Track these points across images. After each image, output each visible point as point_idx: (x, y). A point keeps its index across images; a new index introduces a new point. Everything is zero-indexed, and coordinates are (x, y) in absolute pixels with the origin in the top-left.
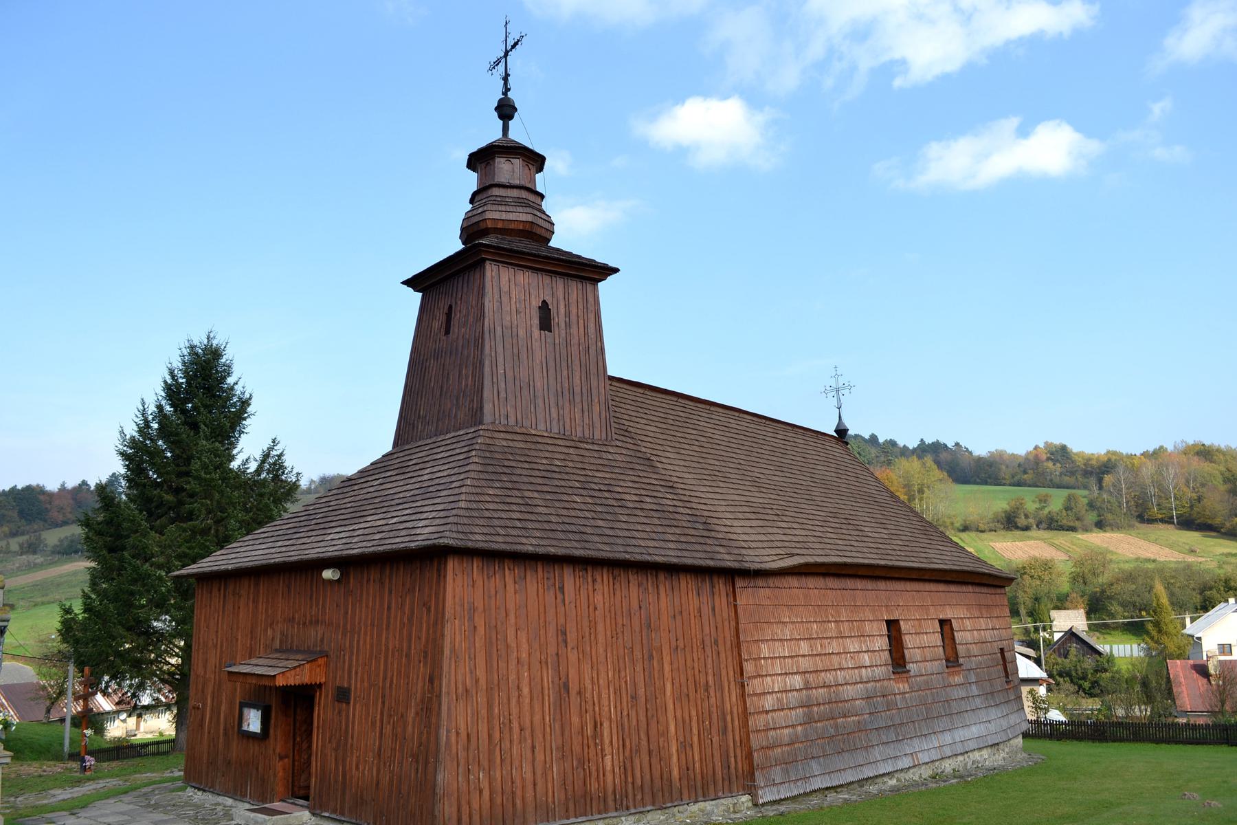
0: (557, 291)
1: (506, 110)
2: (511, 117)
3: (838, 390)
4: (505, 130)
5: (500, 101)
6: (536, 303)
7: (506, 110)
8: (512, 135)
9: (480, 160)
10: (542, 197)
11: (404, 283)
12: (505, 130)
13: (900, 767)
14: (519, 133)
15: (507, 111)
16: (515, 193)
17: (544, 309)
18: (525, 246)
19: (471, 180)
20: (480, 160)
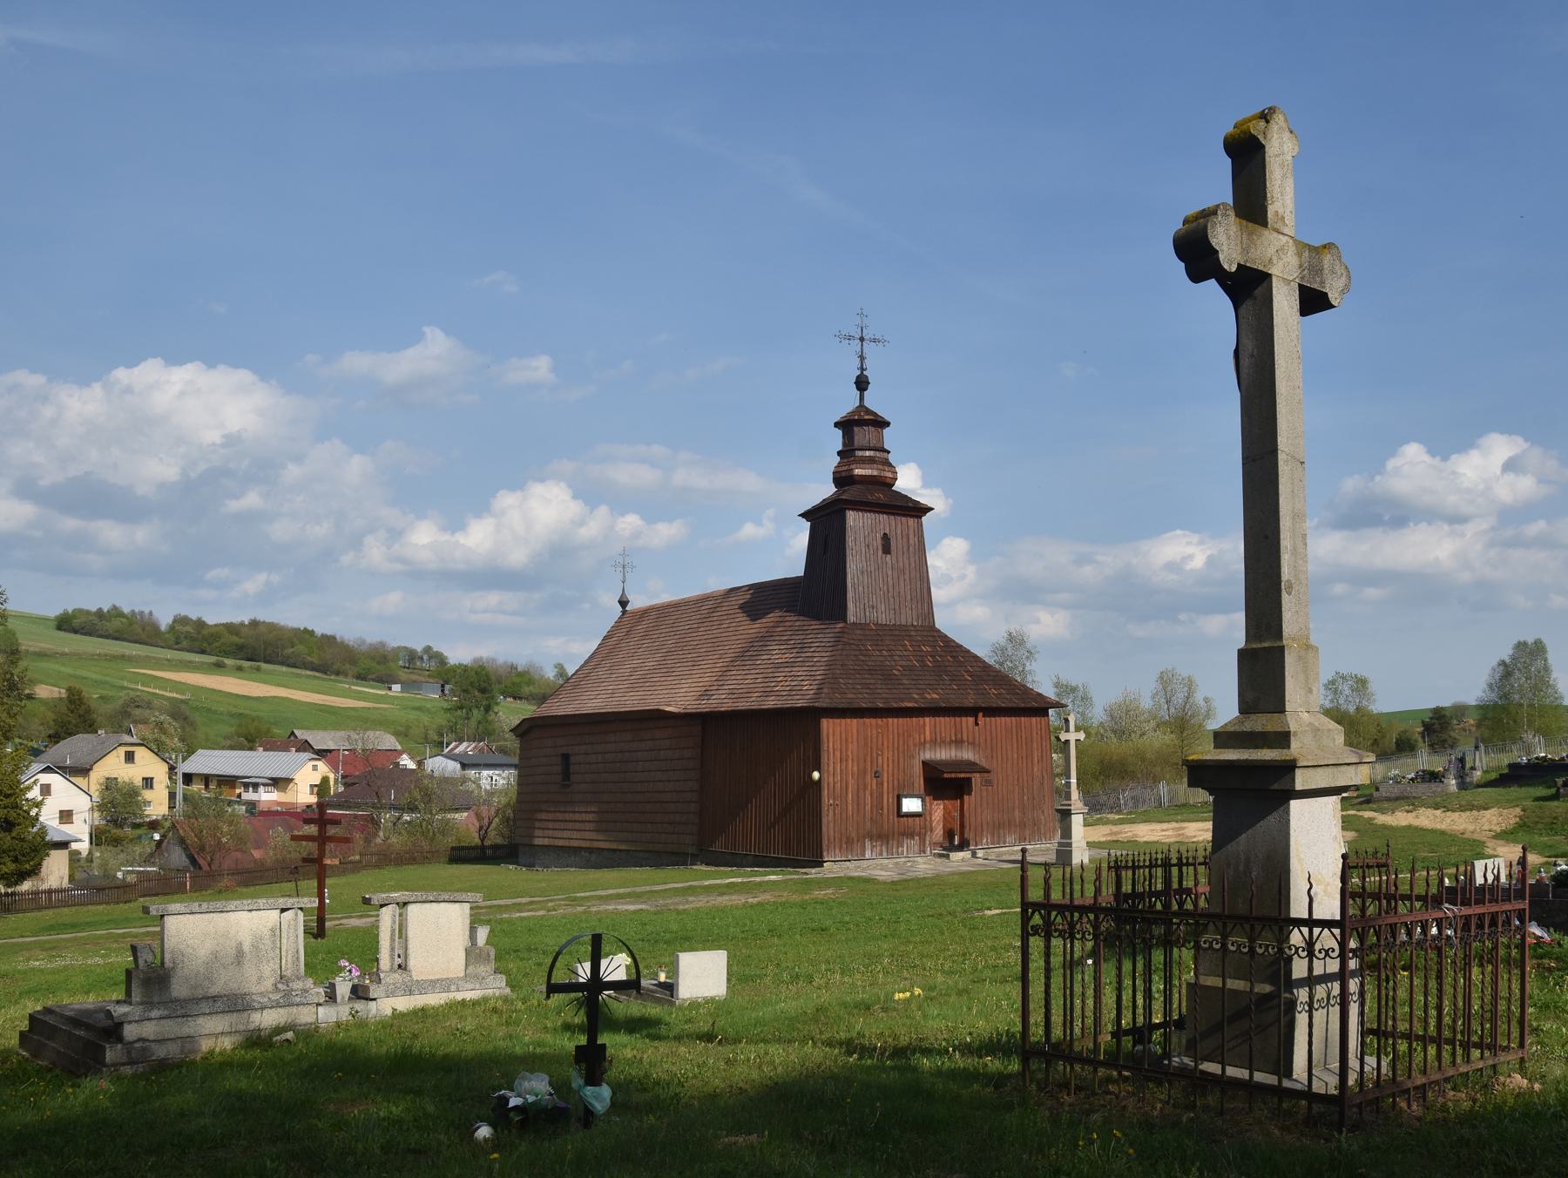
1: (862, 384)
4: (862, 398)
7: (862, 384)
9: (847, 425)
12: (862, 398)
14: (875, 401)
17: (886, 538)
18: (880, 496)
19: (836, 440)
20: (847, 425)
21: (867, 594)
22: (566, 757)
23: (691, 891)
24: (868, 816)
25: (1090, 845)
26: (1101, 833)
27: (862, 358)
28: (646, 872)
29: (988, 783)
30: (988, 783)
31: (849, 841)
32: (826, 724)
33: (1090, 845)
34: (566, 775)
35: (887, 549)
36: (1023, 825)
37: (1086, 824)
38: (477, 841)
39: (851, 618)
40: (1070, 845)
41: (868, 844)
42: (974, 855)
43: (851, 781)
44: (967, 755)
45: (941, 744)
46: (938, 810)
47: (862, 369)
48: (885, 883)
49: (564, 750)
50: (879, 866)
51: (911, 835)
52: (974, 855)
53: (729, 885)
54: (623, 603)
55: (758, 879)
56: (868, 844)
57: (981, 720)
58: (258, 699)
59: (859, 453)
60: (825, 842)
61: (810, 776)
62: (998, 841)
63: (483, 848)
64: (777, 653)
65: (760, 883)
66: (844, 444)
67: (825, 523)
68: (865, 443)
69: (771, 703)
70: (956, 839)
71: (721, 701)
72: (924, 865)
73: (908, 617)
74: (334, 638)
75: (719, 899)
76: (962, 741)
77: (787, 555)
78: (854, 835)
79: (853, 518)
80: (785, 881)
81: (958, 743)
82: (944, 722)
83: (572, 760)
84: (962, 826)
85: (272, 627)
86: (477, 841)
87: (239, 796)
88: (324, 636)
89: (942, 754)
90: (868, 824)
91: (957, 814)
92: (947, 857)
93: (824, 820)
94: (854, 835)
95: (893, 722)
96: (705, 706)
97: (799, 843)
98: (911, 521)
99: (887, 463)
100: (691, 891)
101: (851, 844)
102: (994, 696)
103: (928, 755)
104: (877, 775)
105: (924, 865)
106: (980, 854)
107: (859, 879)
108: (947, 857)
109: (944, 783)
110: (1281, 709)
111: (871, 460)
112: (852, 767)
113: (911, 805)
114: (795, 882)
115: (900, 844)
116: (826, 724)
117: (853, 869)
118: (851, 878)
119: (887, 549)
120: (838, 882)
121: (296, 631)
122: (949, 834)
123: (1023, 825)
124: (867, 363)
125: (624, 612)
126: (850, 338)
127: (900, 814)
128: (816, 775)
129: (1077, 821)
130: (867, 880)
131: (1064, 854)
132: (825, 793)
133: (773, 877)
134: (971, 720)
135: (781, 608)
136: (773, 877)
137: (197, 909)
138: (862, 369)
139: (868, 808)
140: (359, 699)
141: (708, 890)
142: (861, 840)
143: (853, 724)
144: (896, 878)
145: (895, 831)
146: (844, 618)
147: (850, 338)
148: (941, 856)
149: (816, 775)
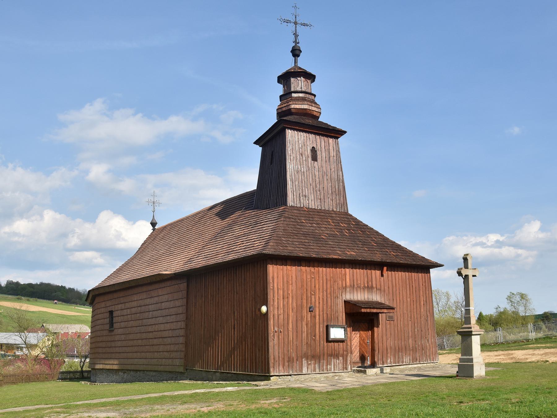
0: (319, 142)
1: (296, 52)
2: (298, 56)
3: (154, 203)
6: (309, 149)
7: (296, 52)
8: (300, 64)
9: (285, 78)
10: (315, 96)
11: (345, 132)
13: (122, 330)
14: (304, 63)
15: (297, 52)
16: (301, 95)
17: (314, 150)
18: (309, 121)
19: (280, 89)
20: (285, 78)
21: (302, 188)
22: (111, 312)
24: (304, 342)
25: (488, 365)
26: (495, 356)
27: (296, 35)
29: (391, 319)
30: (391, 319)
32: (273, 270)
33: (488, 365)
34: (111, 324)
35: (314, 158)
36: (414, 350)
37: (484, 346)
39: (291, 200)
40: (471, 360)
41: (304, 362)
42: (382, 371)
43: (291, 314)
44: (376, 297)
45: (359, 287)
46: (356, 338)
47: (296, 42)
48: (321, 393)
50: (315, 379)
51: (337, 356)
52: (382, 371)
53: (191, 396)
54: (153, 224)
55: (217, 390)
56: (304, 362)
57: (385, 273)
58: (33, 312)
59: (294, 95)
60: (271, 365)
61: (260, 310)
62: (398, 362)
63: (82, 372)
64: (238, 231)
65: (218, 394)
66: (285, 90)
67: (272, 144)
68: (299, 89)
69: (231, 257)
70: (368, 360)
71: (199, 262)
72: (349, 379)
73: (329, 205)
74: (73, 289)
75: (180, 407)
76: (372, 287)
78: (294, 355)
79: (290, 134)
80: (238, 392)
81: (370, 288)
82: (359, 273)
83: (115, 314)
84: (373, 350)
85: (49, 285)
86: (80, 369)
87: (15, 353)
88: (70, 289)
89: (359, 296)
90: (305, 348)
91: (369, 341)
92: (365, 372)
93: (271, 344)
94: (294, 355)
95: (323, 270)
96: (187, 268)
97: (256, 366)
98: (331, 140)
99: (313, 102)
101: (291, 362)
102: (392, 257)
103: (349, 296)
104: (311, 310)
105: (349, 379)
106: (387, 370)
107: (299, 390)
108: (365, 372)
109: (361, 318)
110: (470, 324)
112: (292, 303)
113: (337, 333)
114: (246, 392)
115: (328, 363)
116: (273, 270)
117: (294, 382)
118: (292, 389)
119: (314, 158)
120: (281, 393)
121: (58, 287)
122: (363, 358)
123: (414, 350)
124: (300, 39)
125: (154, 229)
126: (288, 22)
127: (328, 340)
128: (264, 309)
129: (476, 341)
130: (306, 391)
131: (465, 370)
132: (271, 322)
133: (230, 389)
134: (378, 272)
136: (230, 389)
138: (296, 42)
139: (304, 335)
140: (78, 312)
141: (174, 399)
142: (299, 358)
143: (292, 270)
144: (330, 389)
145: (324, 352)
146: (285, 202)
147: (288, 22)
148: (359, 371)
149: (264, 309)
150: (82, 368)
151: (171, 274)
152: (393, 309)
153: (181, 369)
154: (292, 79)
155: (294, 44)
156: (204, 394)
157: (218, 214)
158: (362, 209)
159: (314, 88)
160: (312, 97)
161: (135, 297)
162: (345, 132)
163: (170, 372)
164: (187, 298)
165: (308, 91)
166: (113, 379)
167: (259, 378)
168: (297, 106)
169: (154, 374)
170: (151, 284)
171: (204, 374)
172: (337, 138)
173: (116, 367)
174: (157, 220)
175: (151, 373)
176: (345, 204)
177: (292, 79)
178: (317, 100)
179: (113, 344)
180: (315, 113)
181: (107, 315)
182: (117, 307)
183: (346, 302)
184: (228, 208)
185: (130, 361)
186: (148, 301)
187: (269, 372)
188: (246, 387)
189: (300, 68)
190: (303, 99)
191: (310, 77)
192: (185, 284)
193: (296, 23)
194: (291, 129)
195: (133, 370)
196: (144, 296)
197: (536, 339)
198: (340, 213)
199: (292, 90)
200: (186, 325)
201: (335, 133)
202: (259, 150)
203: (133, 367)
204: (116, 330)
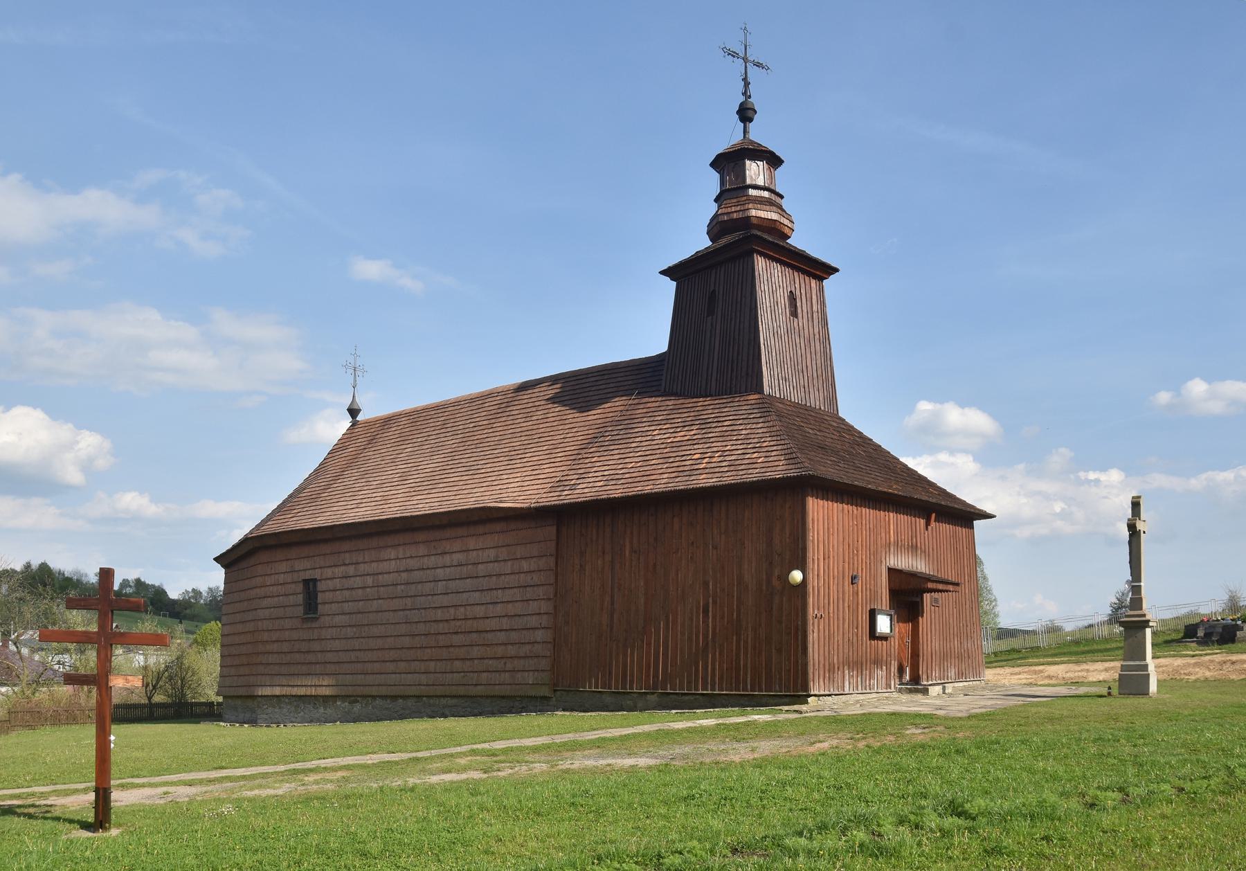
0: (801, 284)
1: (746, 114)
2: (751, 120)
4: (745, 132)
5: (741, 105)
7: (746, 114)
8: (753, 136)
9: (729, 163)
10: (782, 197)
14: (760, 133)
15: (750, 113)
17: (792, 298)
19: (712, 182)
22: (310, 586)
23: (574, 747)
28: (561, 717)
31: (831, 669)
32: (818, 510)
36: (960, 657)
38: (144, 701)
49: (308, 575)
54: (353, 412)
57: (933, 524)
59: (752, 192)
73: (816, 400)
77: (642, 327)
81: (913, 549)
83: (321, 586)
89: (903, 562)
100: (574, 747)
111: (769, 202)
116: (818, 510)
120: (837, 722)
126: (734, 54)
133: (647, 728)
135: (628, 393)
137: (361, 560)
147: (734, 54)
149: (797, 576)
150: (150, 698)
151: (522, 509)
152: (957, 584)
153: (545, 691)
154: (748, 162)
155: (742, 99)
156: (767, 723)
157: (554, 400)
158: (860, 409)
159: (783, 179)
160: (778, 200)
161: (392, 553)
162: (836, 270)
163: (503, 697)
164: (558, 556)
165: (772, 187)
166: (317, 715)
167: (772, 701)
168: (762, 214)
169: (454, 701)
170: (441, 527)
171: (608, 699)
172: (821, 279)
173: (327, 692)
174: (361, 402)
175: (444, 701)
176: (832, 399)
177: (748, 162)
178: (784, 203)
179: (316, 646)
180: (786, 231)
181: (300, 588)
182: (329, 572)
183: (891, 571)
184: (581, 389)
185: (370, 679)
186: (432, 561)
187: (806, 687)
188: (785, 714)
189: (752, 142)
190: (769, 202)
191: (774, 161)
192: (554, 529)
193: (745, 60)
194: (761, 254)
195: (381, 697)
196: (422, 550)
197: (995, 654)
198: (803, 411)
199: (748, 182)
200: (555, 607)
201: (820, 270)
202: (671, 286)
203: (384, 691)
204: (322, 619)
